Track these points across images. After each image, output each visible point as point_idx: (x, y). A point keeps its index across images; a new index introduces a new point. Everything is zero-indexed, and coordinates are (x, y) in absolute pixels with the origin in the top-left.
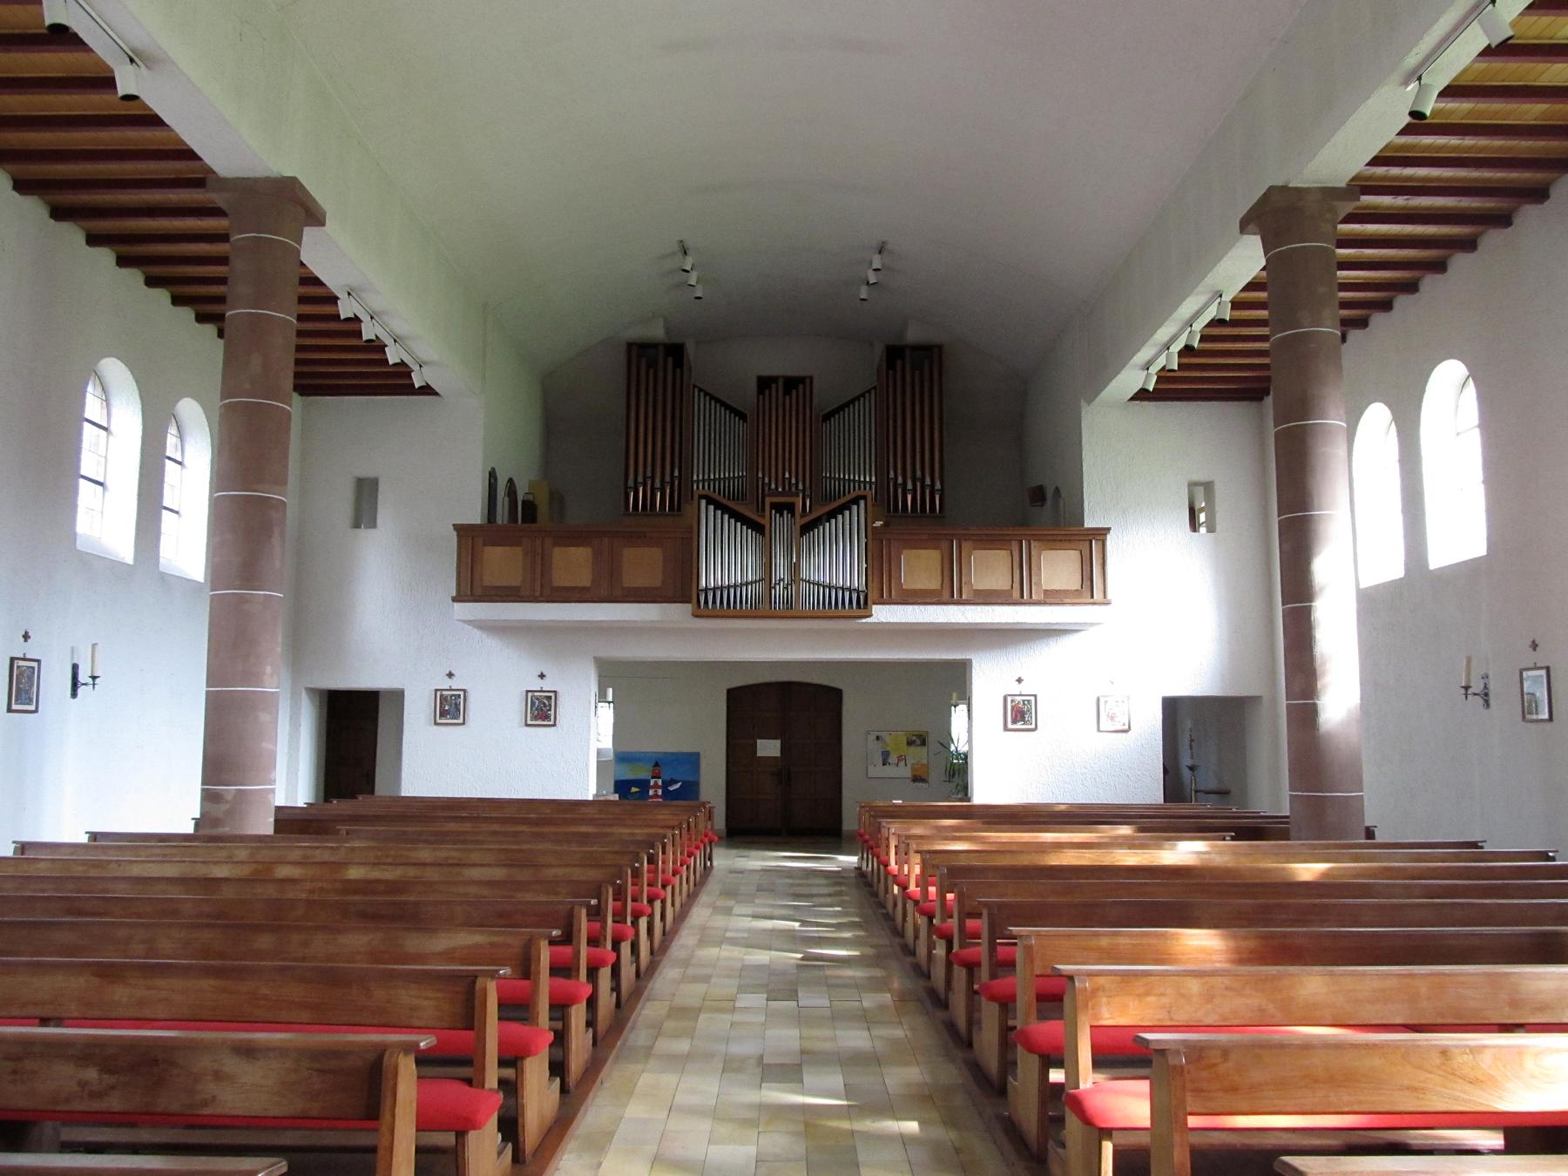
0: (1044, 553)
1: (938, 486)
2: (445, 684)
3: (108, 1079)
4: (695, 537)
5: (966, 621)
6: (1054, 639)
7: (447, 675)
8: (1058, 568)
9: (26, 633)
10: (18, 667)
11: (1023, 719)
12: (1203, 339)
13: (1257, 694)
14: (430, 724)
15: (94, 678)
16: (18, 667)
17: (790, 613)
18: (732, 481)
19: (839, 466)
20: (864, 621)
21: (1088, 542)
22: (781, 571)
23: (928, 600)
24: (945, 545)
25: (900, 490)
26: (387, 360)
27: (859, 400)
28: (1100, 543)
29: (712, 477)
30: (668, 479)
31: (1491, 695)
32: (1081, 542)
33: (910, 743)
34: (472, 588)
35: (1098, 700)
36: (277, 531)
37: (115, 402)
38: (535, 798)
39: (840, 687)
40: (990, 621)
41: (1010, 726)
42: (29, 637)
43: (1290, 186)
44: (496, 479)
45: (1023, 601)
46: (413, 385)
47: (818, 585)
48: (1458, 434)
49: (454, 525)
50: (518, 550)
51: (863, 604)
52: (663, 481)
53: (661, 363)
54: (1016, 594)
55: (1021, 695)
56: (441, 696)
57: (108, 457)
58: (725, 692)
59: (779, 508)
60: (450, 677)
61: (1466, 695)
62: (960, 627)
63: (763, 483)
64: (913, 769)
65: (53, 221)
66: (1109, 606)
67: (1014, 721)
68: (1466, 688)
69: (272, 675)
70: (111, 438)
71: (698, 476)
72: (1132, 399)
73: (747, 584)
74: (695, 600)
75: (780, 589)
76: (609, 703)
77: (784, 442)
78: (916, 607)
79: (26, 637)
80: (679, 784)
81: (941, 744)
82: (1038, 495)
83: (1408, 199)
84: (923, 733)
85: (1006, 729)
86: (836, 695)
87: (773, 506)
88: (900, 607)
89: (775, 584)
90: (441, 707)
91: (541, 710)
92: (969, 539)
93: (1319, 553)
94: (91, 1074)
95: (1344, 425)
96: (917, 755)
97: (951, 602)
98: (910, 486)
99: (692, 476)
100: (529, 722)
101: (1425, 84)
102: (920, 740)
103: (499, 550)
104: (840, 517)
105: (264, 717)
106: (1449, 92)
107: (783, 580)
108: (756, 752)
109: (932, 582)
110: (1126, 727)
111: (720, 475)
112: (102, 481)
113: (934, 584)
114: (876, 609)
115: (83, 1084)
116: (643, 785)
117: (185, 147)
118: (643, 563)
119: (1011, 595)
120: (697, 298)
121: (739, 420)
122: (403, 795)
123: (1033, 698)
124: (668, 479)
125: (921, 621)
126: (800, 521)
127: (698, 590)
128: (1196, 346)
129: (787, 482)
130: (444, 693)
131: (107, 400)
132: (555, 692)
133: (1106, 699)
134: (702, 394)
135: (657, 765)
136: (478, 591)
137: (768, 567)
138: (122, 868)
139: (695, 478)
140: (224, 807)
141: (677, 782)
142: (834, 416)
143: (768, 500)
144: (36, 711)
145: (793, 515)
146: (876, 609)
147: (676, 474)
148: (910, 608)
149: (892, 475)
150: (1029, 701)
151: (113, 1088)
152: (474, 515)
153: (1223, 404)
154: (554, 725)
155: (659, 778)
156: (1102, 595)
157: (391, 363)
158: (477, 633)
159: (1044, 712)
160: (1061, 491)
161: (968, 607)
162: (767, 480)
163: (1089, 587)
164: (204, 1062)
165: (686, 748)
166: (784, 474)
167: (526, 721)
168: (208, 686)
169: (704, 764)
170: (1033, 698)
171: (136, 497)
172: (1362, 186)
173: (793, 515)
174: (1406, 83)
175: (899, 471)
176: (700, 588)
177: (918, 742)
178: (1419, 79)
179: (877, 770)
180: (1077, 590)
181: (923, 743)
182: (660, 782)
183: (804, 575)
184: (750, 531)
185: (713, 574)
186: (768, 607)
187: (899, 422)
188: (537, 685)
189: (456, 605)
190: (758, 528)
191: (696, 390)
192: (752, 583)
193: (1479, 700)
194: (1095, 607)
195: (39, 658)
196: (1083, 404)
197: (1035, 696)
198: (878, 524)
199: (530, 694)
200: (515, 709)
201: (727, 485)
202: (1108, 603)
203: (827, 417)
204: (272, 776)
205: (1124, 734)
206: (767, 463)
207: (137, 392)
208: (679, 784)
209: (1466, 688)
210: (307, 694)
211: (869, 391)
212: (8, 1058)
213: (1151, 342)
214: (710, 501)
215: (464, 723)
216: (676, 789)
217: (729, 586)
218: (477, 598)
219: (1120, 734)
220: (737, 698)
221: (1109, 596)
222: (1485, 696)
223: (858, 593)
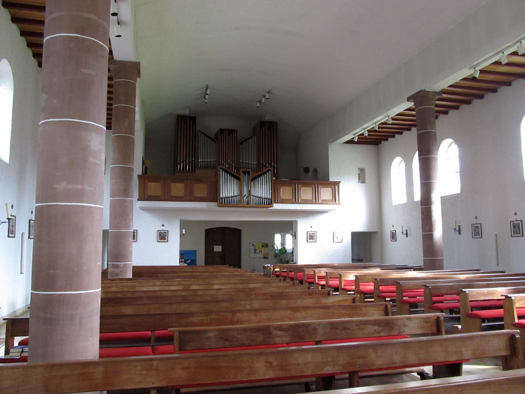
0: (322, 188)
1: (276, 166)
3: (380, 329)
6: (321, 214)
7: (162, 225)
8: (325, 193)
12: (379, 128)
17: (249, 206)
18: (203, 163)
20: (270, 208)
21: (334, 186)
22: (245, 192)
23: (289, 202)
24: (293, 185)
27: (251, 138)
28: (338, 186)
29: (205, 161)
30: (191, 161)
33: (263, 246)
35: (334, 233)
38: (156, 265)
40: (307, 209)
41: (309, 241)
43: (426, 90)
47: (257, 197)
48: (447, 159)
50: (160, 184)
52: (189, 162)
53: (188, 123)
55: (312, 231)
58: (204, 230)
59: (244, 173)
61: (455, 231)
62: (297, 211)
64: (264, 255)
66: (340, 205)
67: (310, 239)
68: (403, 233)
71: (206, 160)
72: (344, 143)
73: (235, 196)
74: (219, 202)
75: (245, 198)
77: (228, 150)
78: (285, 204)
79: (476, 218)
80: (190, 261)
81: (272, 246)
82: (307, 170)
84: (267, 243)
85: (307, 241)
91: (163, 237)
92: (300, 184)
93: (433, 192)
94: (376, 328)
96: (265, 250)
97: (295, 203)
99: (199, 160)
100: (159, 241)
102: (265, 246)
103: (153, 184)
106: (482, 71)
107: (246, 195)
109: (289, 196)
110: (341, 241)
111: (204, 160)
114: (274, 205)
115: (375, 330)
118: (201, 189)
121: (212, 141)
124: (191, 161)
128: (377, 130)
132: (167, 231)
137: (241, 191)
138: (140, 288)
139: (200, 161)
140: (120, 270)
141: (189, 260)
142: (244, 143)
143: (241, 170)
145: (249, 175)
146: (274, 205)
147: (194, 159)
148: (283, 205)
150: (314, 233)
151: (381, 330)
153: (369, 145)
154: (167, 241)
155: (183, 259)
159: (318, 237)
160: (318, 170)
161: (300, 205)
162: (223, 162)
163: (335, 198)
164: (401, 322)
170: (315, 232)
172: (444, 92)
173: (249, 175)
174: (470, 68)
176: (220, 197)
177: (265, 246)
178: (475, 68)
180: (331, 200)
181: (267, 247)
182: (183, 260)
183: (252, 193)
184: (236, 179)
188: (161, 228)
189: (138, 202)
190: (238, 179)
191: (200, 132)
192: (236, 196)
193: (458, 232)
196: (329, 144)
197: (316, 232)
199: (159, 231)
200: (154, 236)
201: (208, 163)
203: (241, 143)
205: (341, 243)
206: (246, 157)
208: (190, 261)
212: (356, 325)
213: (360, 128)
214: (223, 170)
215: (136, 241)
218: (146, 199)
221: (340, 202)
222: (459, 231)
223: (267, 200)
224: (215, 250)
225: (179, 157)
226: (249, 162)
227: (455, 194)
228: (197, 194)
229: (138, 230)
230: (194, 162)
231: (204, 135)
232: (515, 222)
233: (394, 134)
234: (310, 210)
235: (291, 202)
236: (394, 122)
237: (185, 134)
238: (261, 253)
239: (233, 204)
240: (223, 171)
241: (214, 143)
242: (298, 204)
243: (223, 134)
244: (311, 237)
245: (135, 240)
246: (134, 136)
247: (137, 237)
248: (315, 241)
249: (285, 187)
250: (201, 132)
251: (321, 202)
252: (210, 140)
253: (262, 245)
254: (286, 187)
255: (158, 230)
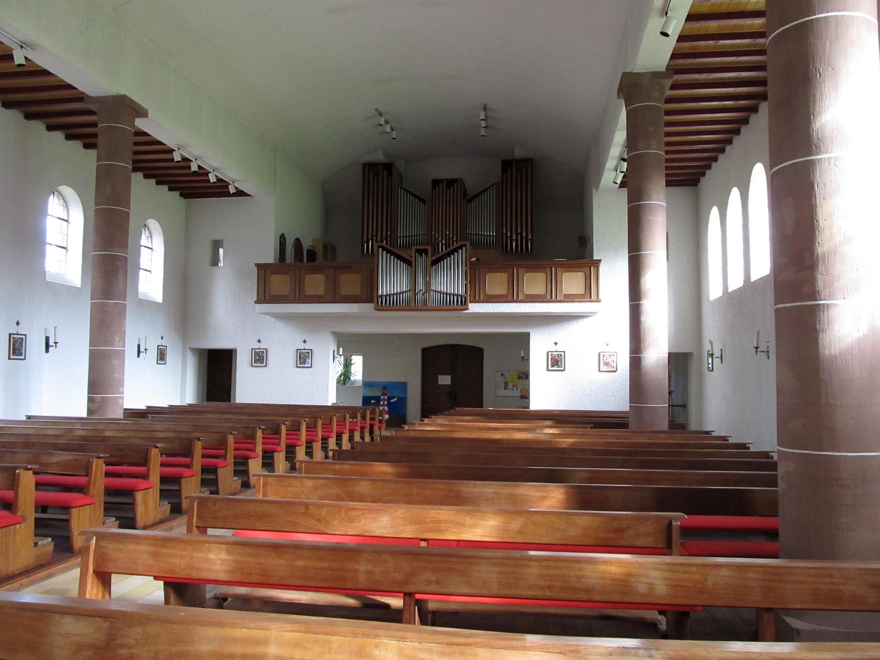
1: (530, 237)
2: (257, 346)
4: (376, 267)
5: (521, 312)
7: (556, 342)
8: (572, 282)
9: (18, 322)
10: (13, 338)
11: (557, 364)
13: (691, 351)
14: (250, 366)
15: (146, 350)
16: (13, 338)
18: (405, 238)
19: (476, 225)
20: (465, 312)
21: (589, 268)
22: (420, 286)
24: (510, 270)
25: (524, 240)
26: (209, 180)
27: (487, 191)
30: (384, 236)
31: (770, 352)
32: (585, 268)
34: (265, 296)
36: (121, 271)
37: (71, 208)
39: (482, 347)
41: (550, 368)
42: (20, 324)
43: (634, 72)
44: (285, 239)
45: (551, 300)
46: (229, 192)
47: (440, 293)
49: (255, 264)
51: (464, 304)
54: (548, 297)
55: (556, 352)
56: (255, 352)
57: (68, 235)
59: (420, 252)
60: (259, 342)
61: (757, 352)
63: (449, 237)
65: (26, 121)
66: (600, 303)
67: (552, 366)
68: (757, 348)
69: (119, 342)
70: (69, 225)
73: (403, 293)
75: (420, 295)
76: (341, 355)
78: (494, 304)
79: (18, 323)
80: (396, 399)
83: (708, 75)
85: (548, 370)
86: (479, 352)
87: (417, 251)
88: (485, 304)
89: (418, 293)
90: (254, 358)
91: (303, 358)
95: (665, 205)
98: (514, 237)
99: (502, 230)
100: (298, 365)
101: (669, 17)
104: (452, 256)
105: (116, 362)
108: (438, 383)
109: (503, 290)
110: (615, 369)
112: (65, 246)
113: (504, 292)
116: (378, 399)
117: (42, 69)
118: (350, 282)
119: (546, 298)
120: (393, 139)
122: (236, 402)
123: (563, 353)
124: (384, 236)
125: (496, 311)
126: (430, 259)
127: (378, 296)
129: (448, 237)
130: (256, 350)
131: (67, 207)
132: (311, 350)
133: (604, 354)
134: (403, 190)
135: (384, 388)
136: (268, 298)
139: (399, 236)
140: (96, 405)
141: (394, 398)
144: (24, 359)
147: (389, 233)
148: (490, 304)
149: (504, 231)
150: (560, 355)
152: (269, 257)
155: (386, 395)
156: (596, 297)
157: (211, 182)
158: (273, 319)
161: (522, 304)
162: (437, 236)
165: (401, 380)
166: (446, 233)
167: (297, 365)
168: (90, 347)
169: (409, 388)
170: (563, 353)
171: (81, 254)
175: (509, 230)
177: (524, 377)
179: (501, 392)
182: (386, 397)
183: (433, 288)
185: (384, 289)
186: (414, 305)
187: (437, 205)
189: (258, 305)
190: (408, 262)
194: (593, 303)
195: (25, 334)
198: (474, 259)
200: (291, 358)
201: (413, 239)
202: (599, 301)
204: (121, 390)
205: (613, 373)
207: (80, 202)
208: (396, 399)
209: (757, 348)
210: (190, 351)
211: (493, 186)
214: (384, 249)
215: (266, 366)
216: (395, 401)
217: (394, 294)
219: (611, 373)
220: (427, 353)
221: (601, 297)
224: (440, 382)
225: (399, 231)
226: (483, 233)
227: (762, 278)
228: (345, 291)
229: (268, 349)
230: (389, 238)
231: (405, 192)
232: (15, 336)
233: (708, 162)
234: (540, 313)
235: (503, 300)
236: (708, 138)
237: (375, 196)
238: (516, 388)
239: (400, 305)
240: (388, 253)
241: (423, 204)
242: (517, 304)
243: (437, 188)
244: (555, 362)
245: (264, 365)
246: (129, 209)
247: (297, 360)
248: (563, 369)
249: (494, 274)
250: (401, 188)
251: (524, 298)
252: (416, 199)
253: (518, 375)
254: (497, 274)
255: (297, 350)
